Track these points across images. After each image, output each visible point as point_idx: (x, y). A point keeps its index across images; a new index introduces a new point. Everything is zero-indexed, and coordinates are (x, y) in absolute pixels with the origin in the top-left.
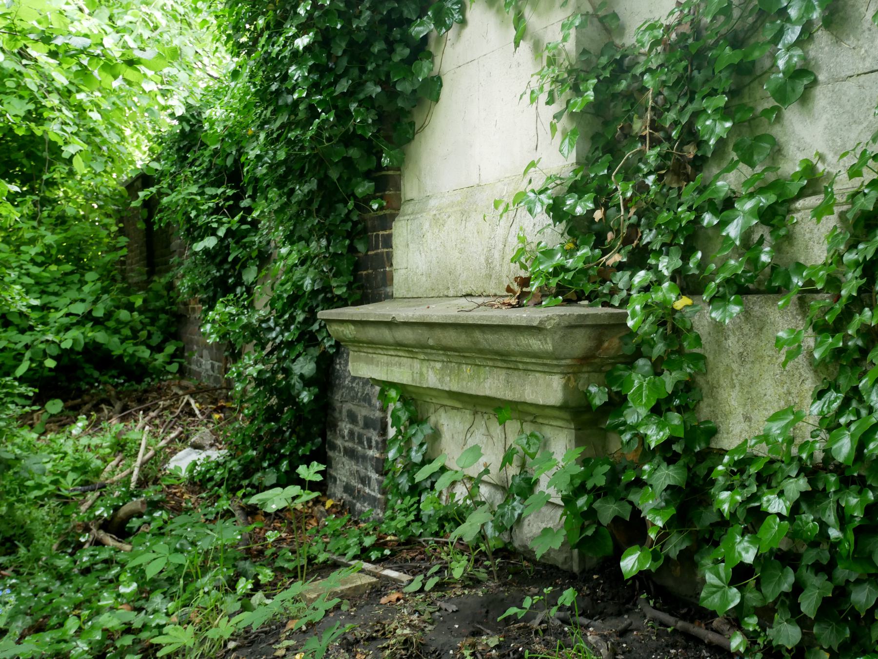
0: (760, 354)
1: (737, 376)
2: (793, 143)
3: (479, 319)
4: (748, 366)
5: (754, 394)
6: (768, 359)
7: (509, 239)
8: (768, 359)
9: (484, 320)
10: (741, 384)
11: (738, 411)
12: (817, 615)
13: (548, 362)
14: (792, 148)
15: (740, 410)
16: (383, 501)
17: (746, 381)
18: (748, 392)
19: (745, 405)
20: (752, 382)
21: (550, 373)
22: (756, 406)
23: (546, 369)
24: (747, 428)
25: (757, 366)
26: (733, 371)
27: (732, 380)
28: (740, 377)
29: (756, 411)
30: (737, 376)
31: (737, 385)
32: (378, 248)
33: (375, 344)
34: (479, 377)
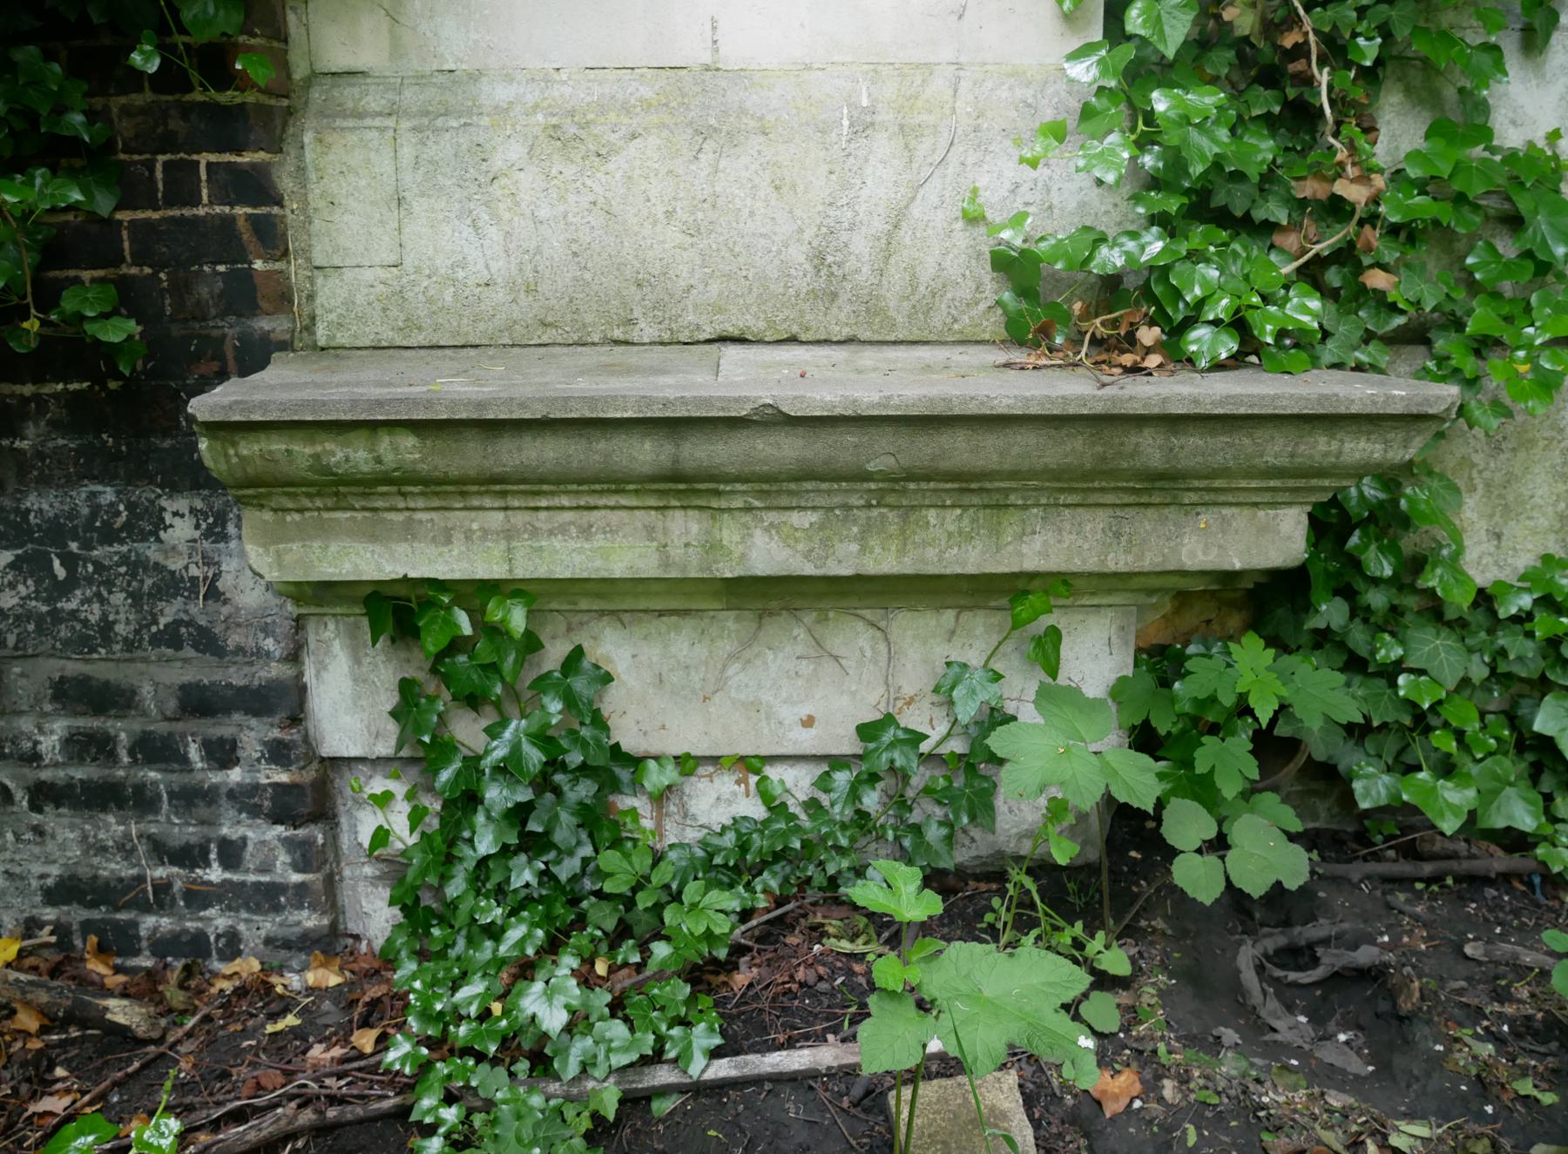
0: (1530, 435)
1: (1480, 472)
2: (1503, 111)
3: (1221, 403)
4: (1502, 457)
5: (1511, 498)
6: (1542, 443)
7: (916, 211)
8: (1542, 443)
9: (1242, 404)
10: (1488, 485)
11: (1477, 526)
12: (1260, 767)
13: (1243, 484)
14: (1500, 119)
15: (1483, 525)
16: (319, 886)
17: (1499, 477)
18: (1500, 496)
19: (1491, 516)
20: (1510, 479)
21: (1273, 505)
22: (1512, 515)
23: (1267, 497)
24: (1492, 549)
25: (1522, 455)
26: (1473, 465)
27: (1471, 479)
28: (1487, 474)
29: (1513, 523)
30: (1480, 472)
31: (1480, 487)
32: (197, 202)
33: (542, 481)
34: (998, 534)
